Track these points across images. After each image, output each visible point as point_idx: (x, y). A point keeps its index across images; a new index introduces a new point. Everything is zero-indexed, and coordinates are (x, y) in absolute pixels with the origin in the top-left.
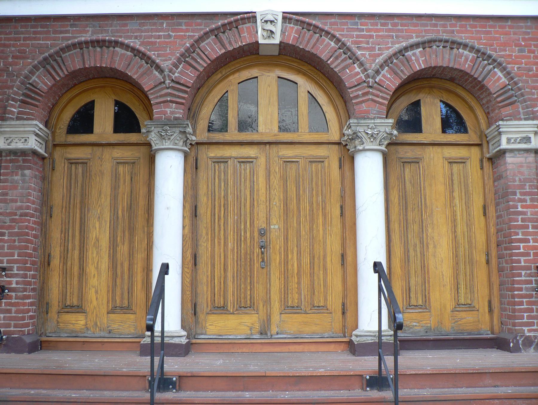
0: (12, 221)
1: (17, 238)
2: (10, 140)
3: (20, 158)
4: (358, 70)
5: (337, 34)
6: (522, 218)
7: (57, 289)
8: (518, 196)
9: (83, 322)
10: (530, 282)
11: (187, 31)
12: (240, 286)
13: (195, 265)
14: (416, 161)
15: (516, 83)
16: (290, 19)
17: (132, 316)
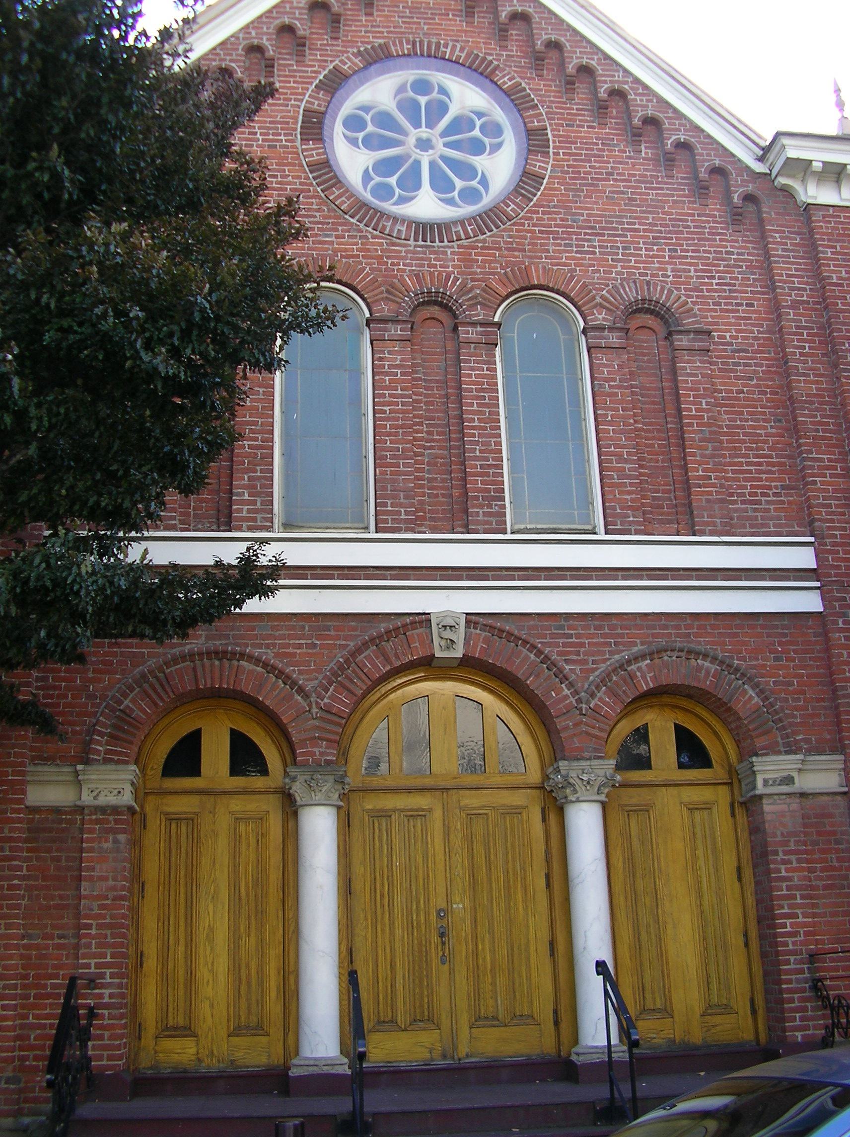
0: (102, 907)
1: (109, 932)
2: (97, 791)
3: (111, 818)
4: (566, 692)
5: (538, 642)
6: (787, 886)
7: (154, 1004)
8: (781, 856)
9: (193, 1051)
10: (801, 971)
11: (338, 638)
12: (414, 990)
13: (351, 962)
14: (645, 809)
15: (772, 705)
16: (476, 623)
17: (264, 1039)
